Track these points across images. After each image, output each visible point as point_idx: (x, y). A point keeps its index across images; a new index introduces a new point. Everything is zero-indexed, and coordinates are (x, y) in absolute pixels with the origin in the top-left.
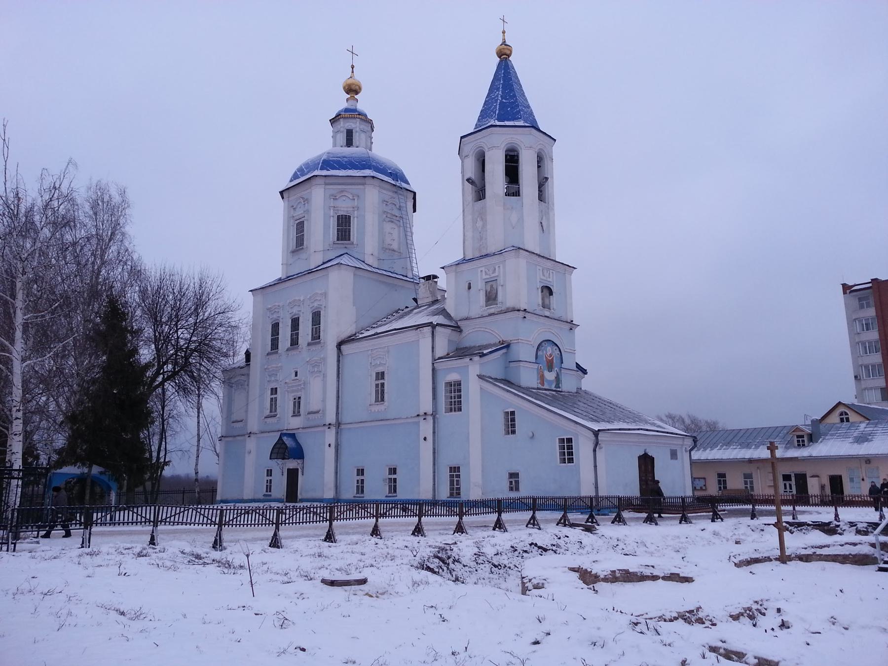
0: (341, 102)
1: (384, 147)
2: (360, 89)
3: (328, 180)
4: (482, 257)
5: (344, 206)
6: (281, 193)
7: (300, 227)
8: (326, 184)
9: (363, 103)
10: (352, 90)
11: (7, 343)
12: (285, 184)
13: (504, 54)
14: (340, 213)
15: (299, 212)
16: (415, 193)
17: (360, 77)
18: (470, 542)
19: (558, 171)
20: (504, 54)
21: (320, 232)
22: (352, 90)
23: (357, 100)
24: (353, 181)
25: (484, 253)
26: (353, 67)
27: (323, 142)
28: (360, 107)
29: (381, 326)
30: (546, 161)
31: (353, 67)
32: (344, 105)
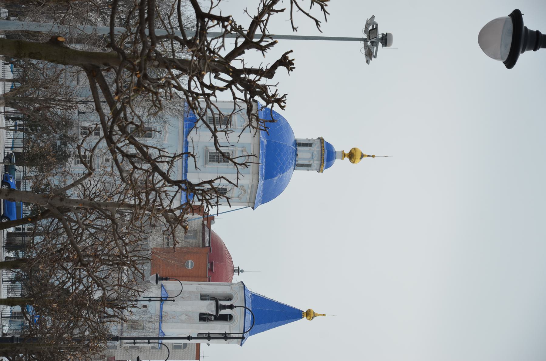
0: (340, 146)
1: (299, 181)
3: (254, 188)
8: (252, 185)
9: (340, 165)
10: (351, 156)
13: (310, 314)
17: (361, 164)
20: (310, 314)
22: (351, 156)
26: (373, 156)
28: (337, 163)
31: (373, 156)
32: (337, 148)
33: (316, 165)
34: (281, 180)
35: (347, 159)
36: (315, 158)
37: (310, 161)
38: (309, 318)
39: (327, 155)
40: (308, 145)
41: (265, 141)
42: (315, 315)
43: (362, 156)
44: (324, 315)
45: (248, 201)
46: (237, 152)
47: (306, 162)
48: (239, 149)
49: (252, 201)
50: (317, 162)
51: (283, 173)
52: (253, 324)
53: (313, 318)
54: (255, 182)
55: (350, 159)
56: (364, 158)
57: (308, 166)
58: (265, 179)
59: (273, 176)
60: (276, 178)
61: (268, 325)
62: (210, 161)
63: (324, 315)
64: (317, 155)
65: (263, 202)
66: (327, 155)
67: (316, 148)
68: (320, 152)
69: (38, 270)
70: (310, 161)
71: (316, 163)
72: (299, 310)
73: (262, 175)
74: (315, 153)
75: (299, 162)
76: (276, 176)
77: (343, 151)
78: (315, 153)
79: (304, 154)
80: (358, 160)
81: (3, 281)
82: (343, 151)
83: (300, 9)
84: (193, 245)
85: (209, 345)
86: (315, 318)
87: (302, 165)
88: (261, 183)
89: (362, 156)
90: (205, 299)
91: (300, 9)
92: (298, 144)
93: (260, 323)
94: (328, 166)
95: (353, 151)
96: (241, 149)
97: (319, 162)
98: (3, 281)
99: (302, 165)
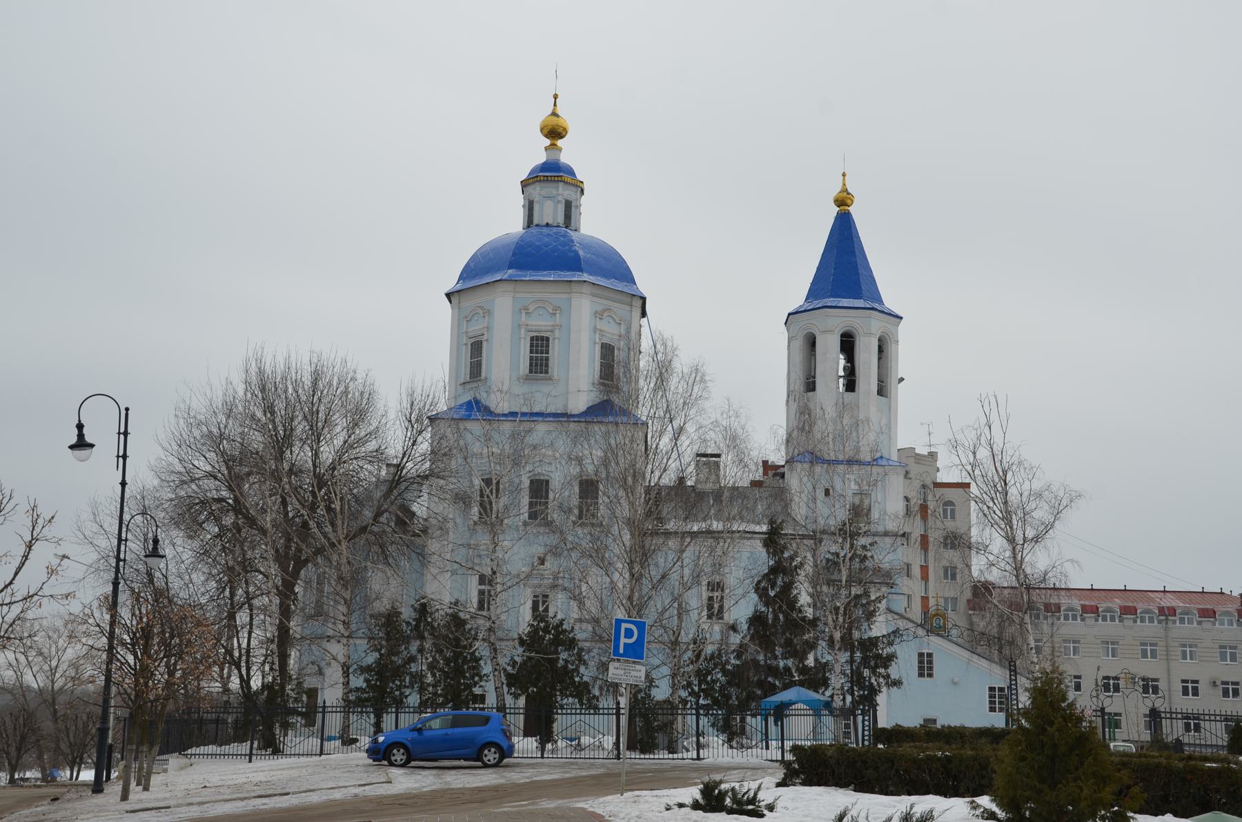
0: (536, 153)
1: (596, 223)
2: (565, 130)
3: (599, 292)
5: (540, 323)
6: (448, 295)
7: (477, 348)
8: (593, 295)
9: (569, 152)
10: (554, 133)
11: (1087, 603)
12: (451, 283)
13: (843, 201)
15: (476, 328)
16: (644, 299)
17: (567, 117)
19: (906, 359)
20: (843, 201)
21: (506, 361)
22: (554, 133)
24: (619, 297)
26: (556, 97)
27: (507, 221)
28: (565, 158)
30: (890, 349)
31: (556, 97)
32: (542, 158)
33: (566, 193)
34: (585, 246)
35: (560, 143)
36: (554, 192)
37: (559, 202)
38: (849, 202)
39: (552, 173)
40: (530, 208)
41: (510, 271)
42: (845, 190)
43: (554, 114)
44: (844, 175)
45: (628, 308)
46: (529, 323)
47: (561, 208)
49: (629, 299)
51: (572, 241)
52: (857, 295)
54: (586, 289)
56: (559, 111)
57: (569, 208)
58: (581, 270)
59: (577, 258)
60: (581, 253)
61: (861, 271)
62: (547, 372)
63: (844, 175)
64: (548, 189)
65: (631, 280)
66: (552, 173)
67: (536, 191)
68: (543, 185)
69: (465, 678)
70: (559, 202)
71: (565, 192)
74: (544, 192)
75: (561, 219)
76: (576, 253)
77: (546, 149)
78: (544, 192)
79: (550, 213)
80: (560, 122)
81: (698, 758)
82: (546, 149)
85: (902, 380)
87: (568, 217)
88: (586, 277)
89: (554, 114)
92: (529, 222)
93: (857, 283)
94: (571, 172)
95: (546, 131)
98: (698, 758)
99: (568, 217)
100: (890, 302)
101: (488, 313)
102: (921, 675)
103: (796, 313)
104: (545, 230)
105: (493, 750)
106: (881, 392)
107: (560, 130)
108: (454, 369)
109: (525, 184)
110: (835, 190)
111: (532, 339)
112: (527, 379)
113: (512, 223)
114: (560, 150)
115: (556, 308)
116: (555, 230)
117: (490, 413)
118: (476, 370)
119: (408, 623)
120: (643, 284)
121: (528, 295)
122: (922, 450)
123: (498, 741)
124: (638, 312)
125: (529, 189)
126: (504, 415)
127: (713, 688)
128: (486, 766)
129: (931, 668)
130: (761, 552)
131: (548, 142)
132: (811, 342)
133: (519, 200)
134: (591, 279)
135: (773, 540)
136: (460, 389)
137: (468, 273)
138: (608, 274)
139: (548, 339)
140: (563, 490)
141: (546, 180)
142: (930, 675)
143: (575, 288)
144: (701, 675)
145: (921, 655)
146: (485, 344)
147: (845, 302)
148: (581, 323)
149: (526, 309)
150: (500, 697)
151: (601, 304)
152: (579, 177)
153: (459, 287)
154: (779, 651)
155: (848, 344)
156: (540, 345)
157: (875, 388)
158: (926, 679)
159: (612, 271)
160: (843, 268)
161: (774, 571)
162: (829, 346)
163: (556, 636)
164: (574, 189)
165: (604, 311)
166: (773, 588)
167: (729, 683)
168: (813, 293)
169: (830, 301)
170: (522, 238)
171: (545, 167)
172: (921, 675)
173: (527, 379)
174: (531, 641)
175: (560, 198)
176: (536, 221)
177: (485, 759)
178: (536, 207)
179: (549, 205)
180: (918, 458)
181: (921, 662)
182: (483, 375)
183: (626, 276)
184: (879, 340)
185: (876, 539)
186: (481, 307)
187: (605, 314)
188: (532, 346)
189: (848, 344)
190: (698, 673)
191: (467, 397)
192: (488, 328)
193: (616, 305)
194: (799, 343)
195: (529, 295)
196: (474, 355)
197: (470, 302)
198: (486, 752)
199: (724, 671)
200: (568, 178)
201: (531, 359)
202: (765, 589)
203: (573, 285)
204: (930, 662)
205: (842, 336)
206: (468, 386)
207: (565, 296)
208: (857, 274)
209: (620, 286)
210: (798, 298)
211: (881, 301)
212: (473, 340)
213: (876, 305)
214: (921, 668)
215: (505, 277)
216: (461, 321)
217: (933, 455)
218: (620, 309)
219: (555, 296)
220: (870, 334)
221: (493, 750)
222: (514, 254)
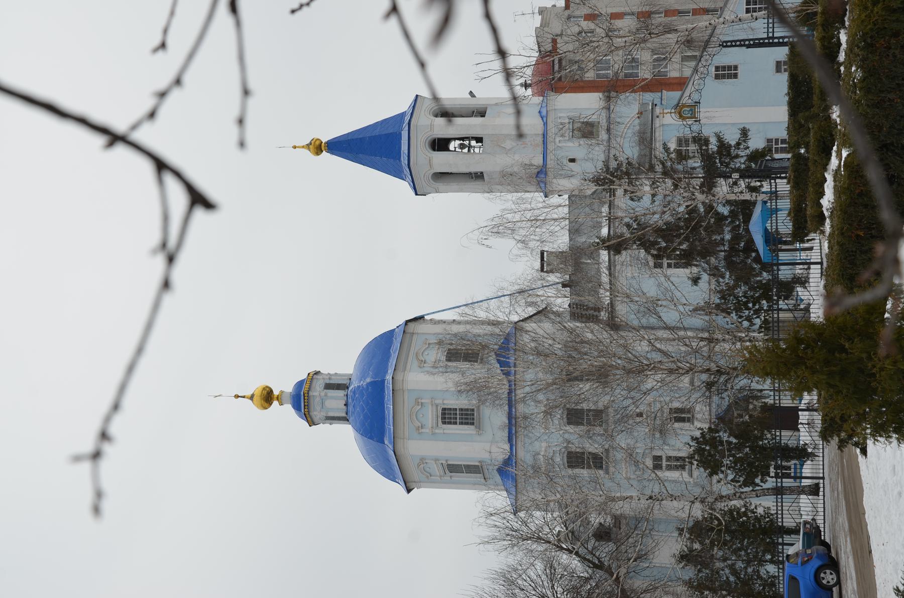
0: (285, 412)
1: (344, 362)
3: (401, 367)
4: (545, 143)
5: (430, 416)
7: (454, 469)
8: (404, 370)
9: (284, 385)
10: (268, 397)
12: (398, 488)
13: (317, 148)
14: (444, 358)
15: (436, 469)
16: (407, 322)
17: (254, 386)
18: (635, 109)
20: (317, 148)
22: (268, 397)
23: (282, 392)
24: (405, 345)
25: (540, 139)
26: (237, 396)
28: (289, 388)
29: (833, 491)
31: (237, 396)
32: (288, 408)
33: (318, 388)
35: (276, 392)
36: (318, 399)
37: (326, 395)
38: (318, 143)
39: (302, 400)
41: (386, 442)
42: (308, 146)
43: (252, 398)
44: (295, 147)
45: (415, 337)
46: (430, 426)
47: (331, 393)
48: (427, 431)
49: (408, 336)
50: (315, 394)
51: (359, 387)
53: (311, 143)
54: (399, 377)
55: (271, 391)
56: (249, 394)
58: (383, 381)
60: (368, 380)
62: (473, 410)
63: (295, 147)
66: (302, 400)
67: (316, 414)
68: (312, 409)
70: (326, 395)
71: (318, 390)
72: (333, 154)
73: (388, 388)
74: (318, 408)
75: (341, 393)
76: (368, 384)
77: (281, 404)
78: (318, 408)
79: (336, 402)
80: (258, 393)
82: (281, 404)
83: (488, 16)
84: (846, 186)
86: (308, 142)
88: (389, 377)
89: (252, 398)
90: (476, 173)
91: (488, 16)
92: (344, 419)
93: (388, 136)
94: (300, 384)
95: (266, 405)
96: (423, 430)
97: (311, 393)
100: (403, 106)
101: (422, 460)
102: (735, 76)
103: (415, 188)
104: (351, 408)
105: (822, 575)
106: (482, 114)
107: (265, 392)
108: (474, 486)
109: (312, 423)
110: (308, 154)
111: (444, 423)
112: (479, 428)
113: (345, 435)
114: (282, 392)
115: (417, 402)
116: (350, 400)
117: (509, 459)
118: (473, 469)
119: (700, 571)
120: (393, 321)
121: (406, 426)
122: (537, 20)
123: (813, 571)
124: (420, 328)
125: (316, 420)
126: (511, 449)
127: (752, 297)
128: (838, 583)
129: (729, 68)
130: (625, 256)
131: (275, 403)
132: (441, 176)
133: (324, 428)
134: (390, 371)
135: (616, 246)
136: (490, 482)
137: (389, 474)
138: (386, 356)
139: (444, 409)
140: (577, 437)
141: (307, 406)
142: (736, 68)
143: (398, 386)
144: (739, 307)
145: (717, 77)
146: (450, 463)
147: (404, 148)
148: (426, 382)
149: (418, 428)
150: (765, 492)
151: (412, 363)
152: (304, 376)
153: (402, 483)
154: (718, 237)
155: (440, 145)
156: (448, 416)
157: (479, 120)
158: (739, 71)
159: (382, 350)
160: (375, 147)
161: (646, 245)
162: (441, 161)
163: (706, 442)
164: (315, 381)
165: (418, 359)
166: (658, 243)
167: (746, 283)
168: (397, 173)
169: (404, 161)
170: (357, 430)
171: (297, 407)
172: (735, 76)
173: (479, 428)
174: (712, 466)
175: (323, 394)
176: (344, 415)
177: (832, 583)
178: (331, 414)
179: (329, 404)
180: (544, 24)
181: (723, 77)
182: (477, 464)
183: (387, 338)
184: (436, 116)
185: (611, 156)
186: (419, 465)
187: (421, 358)
188: (450, 423)
189: (440, 145)
190: (738, 310)
191: (498, 478)
192: (436, 460)
193: (412, 349)
194: (440, 185)
195: (406, 425)
196: (456, 471)
197: (414, 473)
198: (824, 582)
199: (736, 286)
200: (305, 387)
201: (461, 423)
202: (659, 249)
203: (396, 388)
204: (724, 68)
205: (434, 150)
206: (487, 476)
207: (406, 394)
208: (380, 136)
209: (396, 344)
210: (403, 186)
211: (403, 115)
212: (447, 471)
213: (407, 118)
214: (730, 76)
215: (391, 447)
216: (429, 480)
217: (542, 11)
218: (417, 344)
219: (407, 404)
220: (432, 126)
221: (822, 575)
222: (371, 438)
